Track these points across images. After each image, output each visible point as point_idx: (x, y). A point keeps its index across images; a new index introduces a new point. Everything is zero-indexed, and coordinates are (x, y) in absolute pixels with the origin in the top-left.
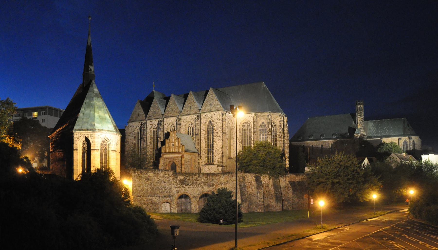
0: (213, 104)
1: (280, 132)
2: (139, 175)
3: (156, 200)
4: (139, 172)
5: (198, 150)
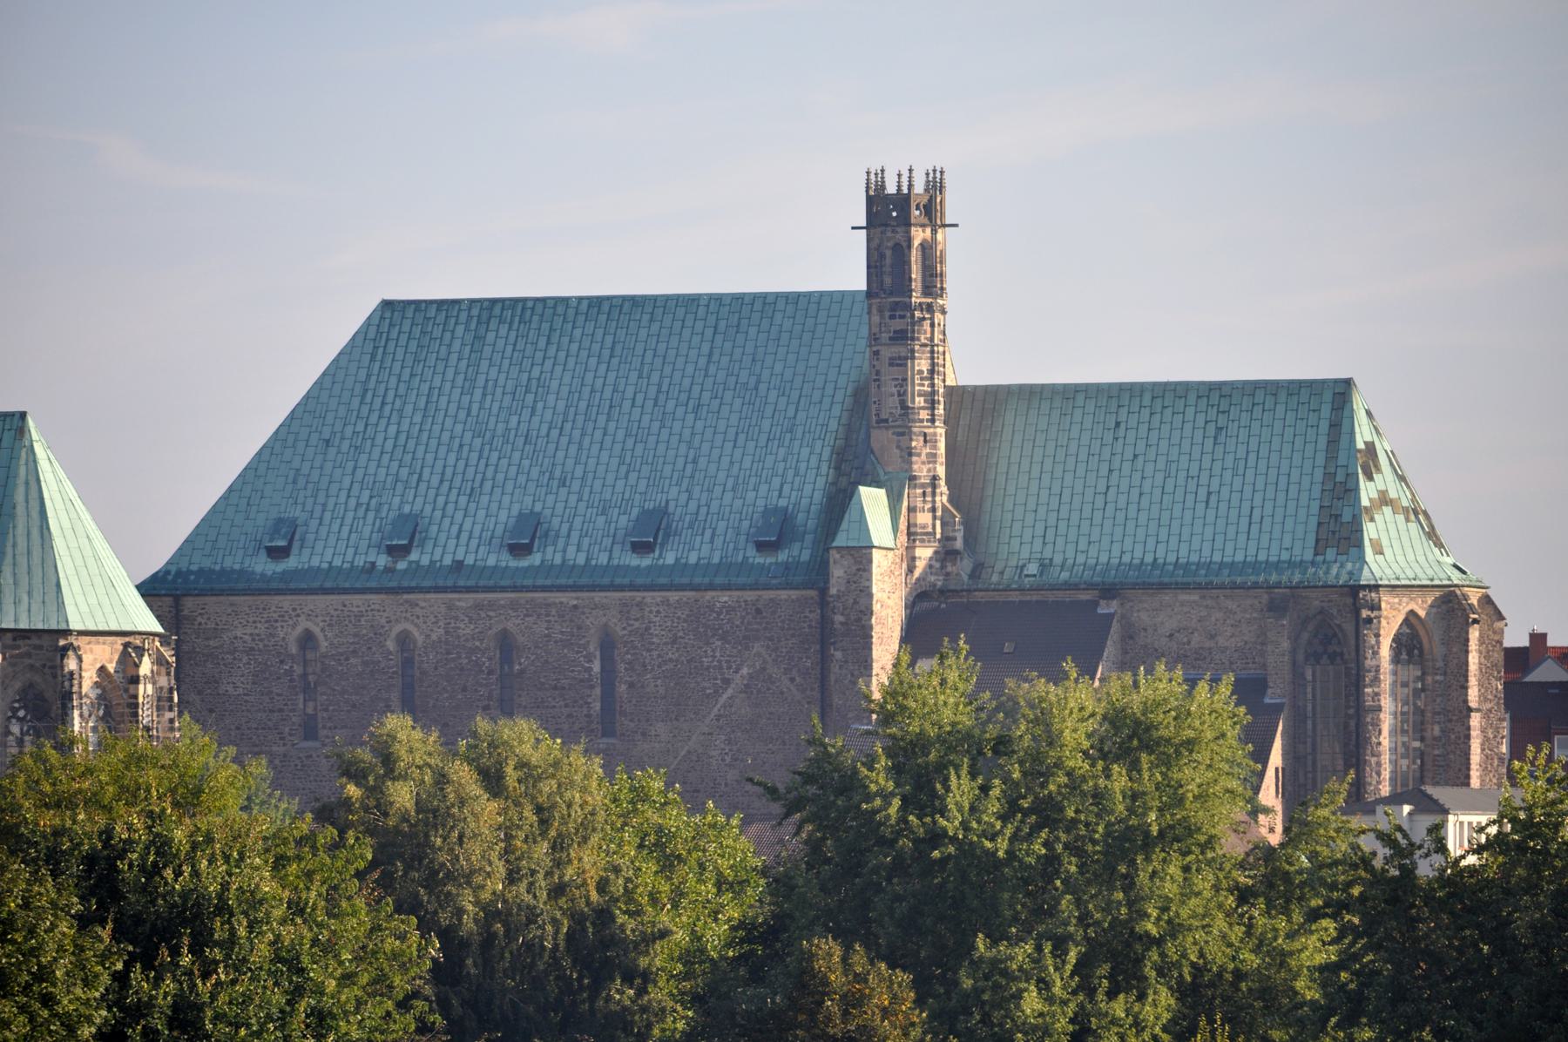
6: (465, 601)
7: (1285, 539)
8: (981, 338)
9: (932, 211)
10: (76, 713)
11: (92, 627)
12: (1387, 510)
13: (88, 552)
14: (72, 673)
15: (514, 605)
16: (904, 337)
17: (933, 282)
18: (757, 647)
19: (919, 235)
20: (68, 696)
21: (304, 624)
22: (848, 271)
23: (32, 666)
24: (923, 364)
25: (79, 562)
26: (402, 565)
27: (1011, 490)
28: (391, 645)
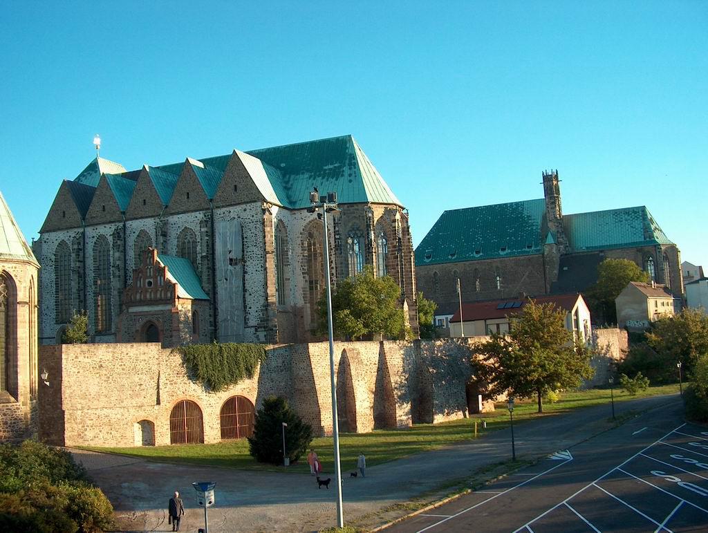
0: (240, 186)
2: (76, 357)
3: (119, 416)
4: (79, 351)
5: (208, 294)
6: (468, 263)
7: (639, 238)
8: (570, 205)
9: (556, 176)
10: (372, 232)
11: (377, 201)
13: (374, 178)
14: (370, 217)
15: (478, 263)
16: (554, 203)
17: (558, 193)
18: (530, 267)
19: (555, 183)
20: (368, 226)
21: (435, 270)
22: (539, 193)
23: (355, 217)
24: (557, 208)
25: (371, 181)
26: (453, 258)
28: (452, 273)
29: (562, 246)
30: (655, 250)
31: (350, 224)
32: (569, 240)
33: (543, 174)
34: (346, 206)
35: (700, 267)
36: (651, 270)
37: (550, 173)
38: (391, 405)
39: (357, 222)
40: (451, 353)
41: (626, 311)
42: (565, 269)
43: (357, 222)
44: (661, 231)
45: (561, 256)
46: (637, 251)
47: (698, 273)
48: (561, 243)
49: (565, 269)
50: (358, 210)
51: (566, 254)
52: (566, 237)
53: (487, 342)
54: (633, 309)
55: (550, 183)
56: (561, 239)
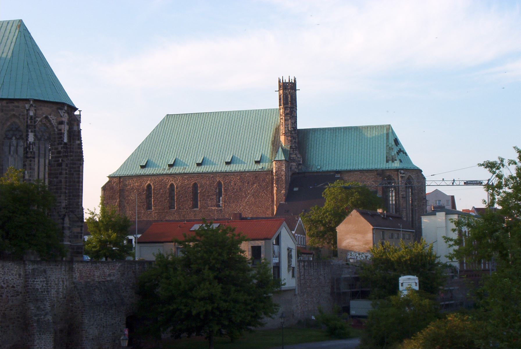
1: (59, 152)
12: (402, 153)
21: (149, 182)
23: (14, 115)
27: (312, 151)
29: (295, 164)
30: (398, 175)
31: (9, 124)
32: (304, 161)
33: (280, 82)
34: (5, 102)
35: (453, 197)
36: (392, 200)
37: (287, 81)
38: (29, 335)
39: (17, 121)
40: (112, 278)
41: (348, 241)
42: (296, 189)
43: (17, 121)
44: (406, 153)
45: (293, 174)
46: (378, 174)
47: (450, 203)
48: (293, 160)
49: (296, 189)
50: (19, 107)
51: (298, 173)
52: (300, 153)
53: (455, 251)
54: (356, 239)
55: (288, 91)
56: (294, 156)
